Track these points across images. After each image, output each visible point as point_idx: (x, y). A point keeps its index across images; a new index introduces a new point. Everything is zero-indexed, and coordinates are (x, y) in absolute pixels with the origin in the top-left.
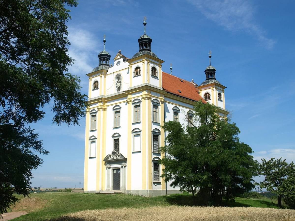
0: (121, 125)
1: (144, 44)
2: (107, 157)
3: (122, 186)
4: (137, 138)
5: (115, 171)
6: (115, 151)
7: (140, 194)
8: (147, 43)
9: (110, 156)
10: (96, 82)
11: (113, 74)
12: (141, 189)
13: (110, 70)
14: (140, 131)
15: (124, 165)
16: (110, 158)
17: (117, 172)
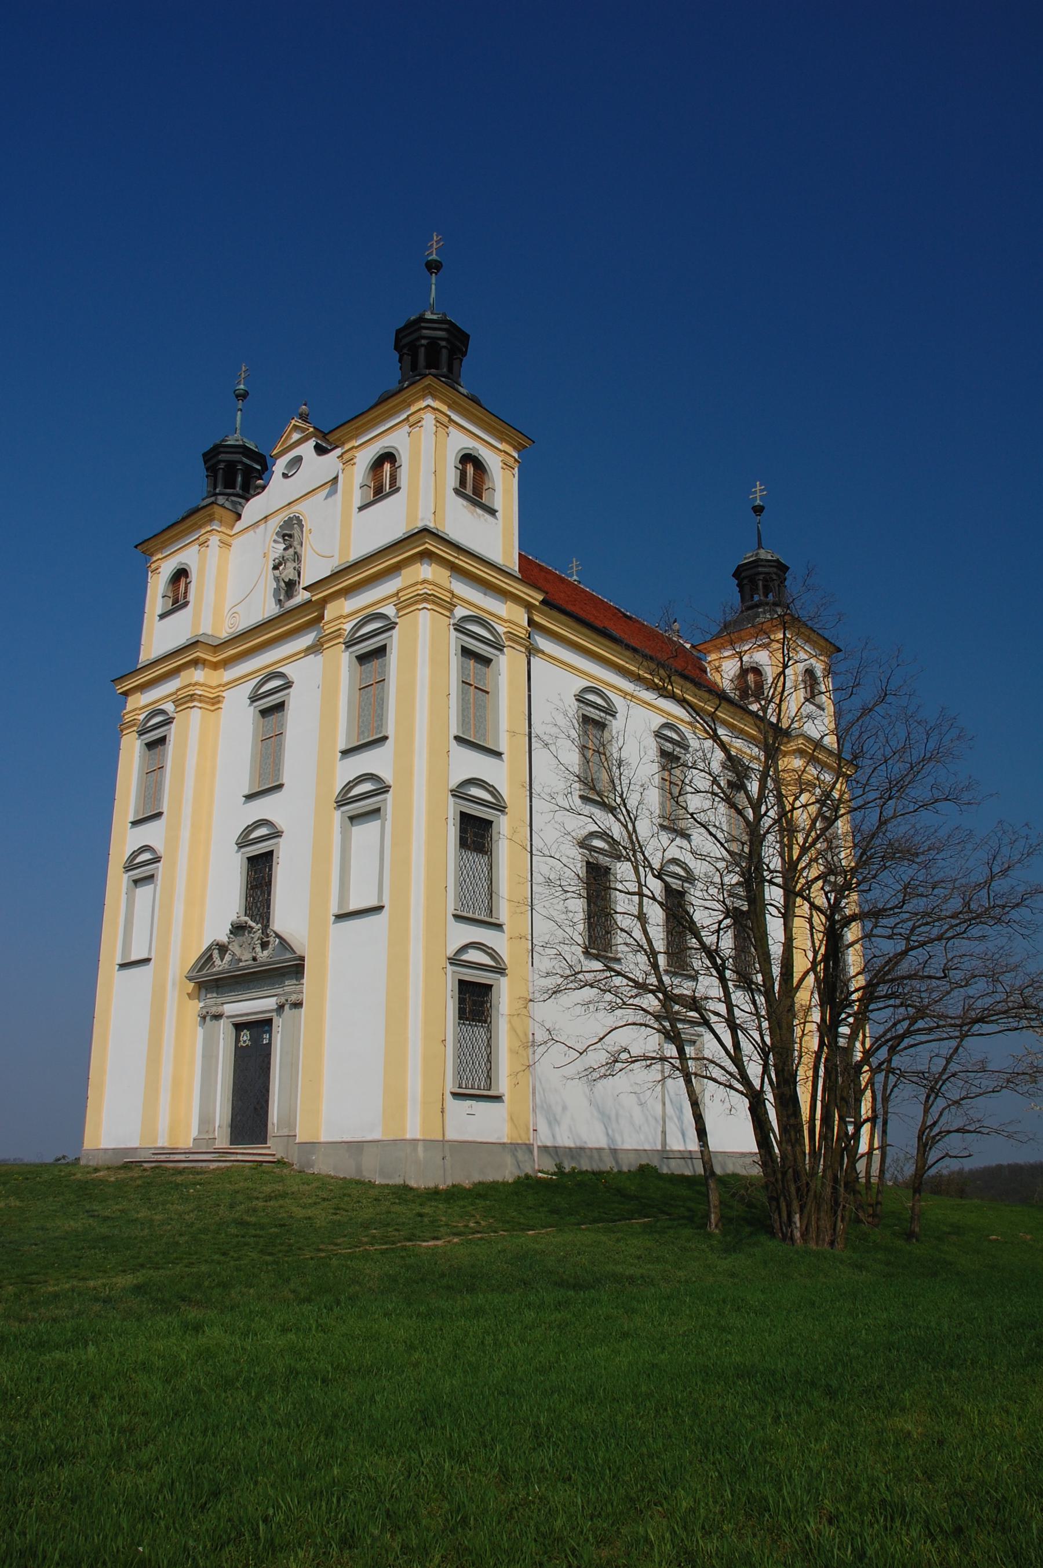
0: (285, 780)
1: (423, 349)
2: (206, 959)
3: (275, 1121)
4: (366, 833)
5: (245, 1036)
6: (247, 918)
7: (374, 1172)
8: (443, 343)
9: (223, 949)
10: (181, 574)
11: (262, 527)
12: (376, 1135)
13: (254, 508)
14: (385, 789)
15: (293, 998)
16: (218, 962)
17: (256, 1040)
